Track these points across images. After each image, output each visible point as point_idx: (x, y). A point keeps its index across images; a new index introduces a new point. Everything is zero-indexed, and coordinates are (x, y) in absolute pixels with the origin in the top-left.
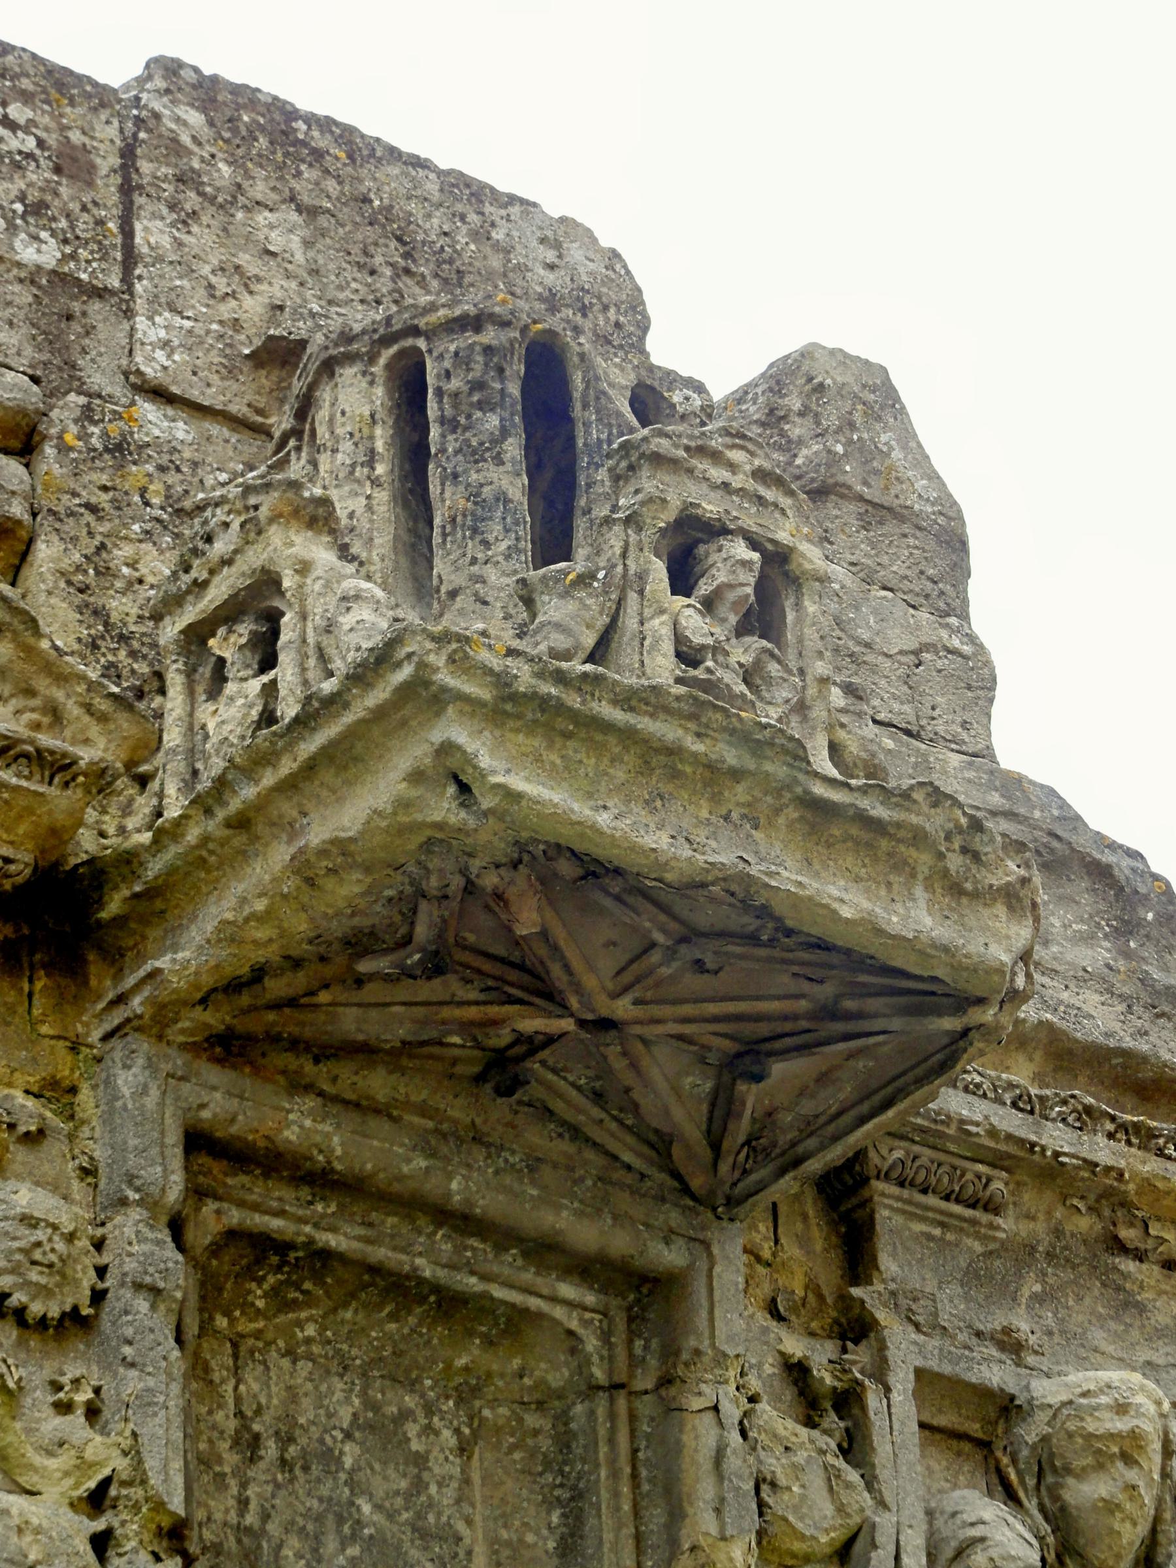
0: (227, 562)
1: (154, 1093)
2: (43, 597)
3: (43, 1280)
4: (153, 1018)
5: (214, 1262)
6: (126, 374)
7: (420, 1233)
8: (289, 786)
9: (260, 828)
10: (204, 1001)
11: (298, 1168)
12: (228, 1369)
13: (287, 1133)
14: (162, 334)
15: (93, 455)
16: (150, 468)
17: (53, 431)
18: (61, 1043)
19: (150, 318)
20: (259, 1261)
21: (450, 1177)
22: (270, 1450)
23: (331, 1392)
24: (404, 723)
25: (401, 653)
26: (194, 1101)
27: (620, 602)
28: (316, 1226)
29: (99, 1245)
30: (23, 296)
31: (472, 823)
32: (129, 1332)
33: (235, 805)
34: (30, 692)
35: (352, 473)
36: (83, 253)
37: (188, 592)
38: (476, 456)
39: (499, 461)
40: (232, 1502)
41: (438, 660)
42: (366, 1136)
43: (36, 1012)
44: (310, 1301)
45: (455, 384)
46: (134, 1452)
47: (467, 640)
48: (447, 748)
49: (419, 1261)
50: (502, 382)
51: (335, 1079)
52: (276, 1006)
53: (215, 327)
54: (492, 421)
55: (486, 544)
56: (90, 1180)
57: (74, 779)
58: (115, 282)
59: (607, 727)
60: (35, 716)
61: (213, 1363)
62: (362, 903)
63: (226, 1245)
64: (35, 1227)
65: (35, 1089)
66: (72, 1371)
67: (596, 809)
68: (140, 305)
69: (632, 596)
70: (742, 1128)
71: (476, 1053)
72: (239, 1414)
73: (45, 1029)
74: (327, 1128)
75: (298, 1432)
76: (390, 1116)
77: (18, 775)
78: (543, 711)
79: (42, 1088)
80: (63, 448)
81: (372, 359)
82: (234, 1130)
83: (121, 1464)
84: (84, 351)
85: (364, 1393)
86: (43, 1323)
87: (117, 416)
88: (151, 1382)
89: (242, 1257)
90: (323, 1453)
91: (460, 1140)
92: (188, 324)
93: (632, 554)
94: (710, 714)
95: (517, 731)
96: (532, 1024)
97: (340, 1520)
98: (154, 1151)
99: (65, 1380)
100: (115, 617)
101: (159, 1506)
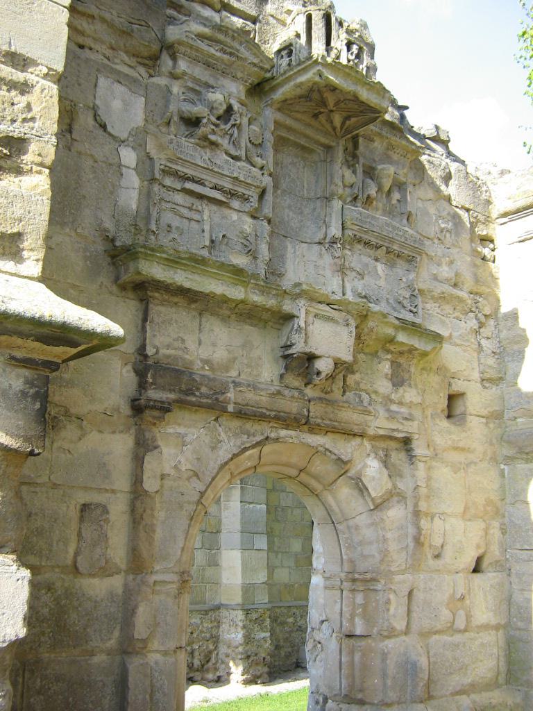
22: (280, 166)
29: (263, 135)
70: (345, 127)
81: (304, 13)
86: (255, 145)
94: (117, 20)
96: (322, 110)
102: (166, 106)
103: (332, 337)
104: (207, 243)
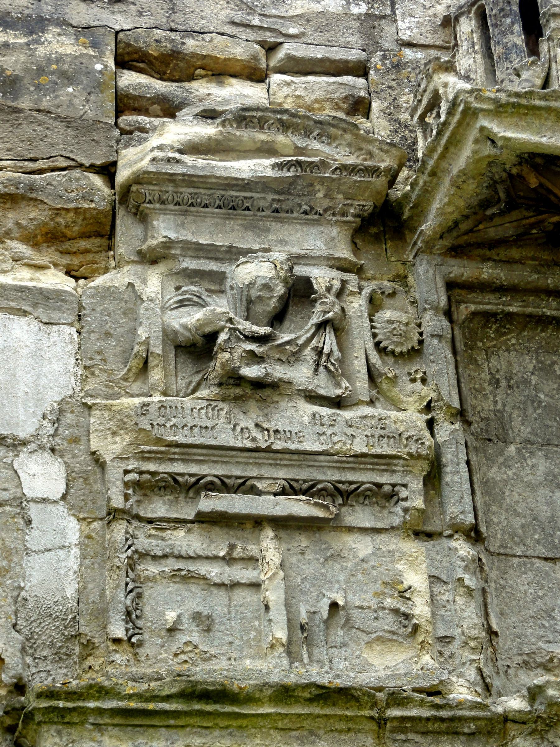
0: (425, 91)
1: (431, 272)
2: (375, 120)
3: (399, 340)
4: (426, 247)
5: (472, 325)
6: (397, 41)
7: (543, 300)
8: (443, 156)
9: (439, 174)
10: (441, 237)
11: (491, 287)
12: (484, 359)
13: (483, 276)
14: (408, 25)
15: (388, 70)
16: (409, 70)
17: (372, 65)
18: (399, 263)
19: (403, 21)
20: (488, 321)
21: (547, 279)
22: (504, 383)
23: (524, 360)
24: (468, 124)
25: (459, 101)
26: (447, 271)
27: (550, 68)
28: (503, 305)
29: (419, 325)
30: (356, 24)
31: (499, 152)
32: (431, 351)
33: (429, 168)
34: (361, 149)
35: (468, 52)
36: (376, 6)
37: (418, 105)
38: (504, 34)
39: (512, 33)
40: (491, 403)
41: (471, 99)
42: (513, 271)
43: (388, 254)
44: (510, 331)
45: (494, 11)
46: (437, 390)
47: (480, 90)
48: (482, 129)
49: (544, 310)
50: (510, 6)
51: (498, 255)
52: (466, 233)
53: (427, 18)
54: (509, 20)
55: (511, 62)
56: (415, 305)
57: (380, 173)
58: (389, 12)
59: (539, 108)
60: (364, 156)
61: (478, 358)
62: (478, 190)
63: (473, 318)
64: (393, 323)
65: (392, 279)
66: (414, 368)
67: (541, 137)
68: (399, 17)
69: (553, 64)
71: (543, 234)
72: (490, 373)
73: (393, 259)
74: (498, 271)
75: (513, 376)
76: (521, 263)
77: (360, 177)
78: (514, 108)
79: (394, 278)
80: (377, 70)
81: (469, 12)
82: (464, 278)
83: (433, 395)
84: (381, 37)
85: (537, 358)
87: (395, 55)
88: (441, 366)
89: (481, 321)
90: (524, 381)
91: (549, 266)
92: (417, 20)
93: (551, 50)
95: (507, 117)
97: (533, 402)
98: (434, 291)
99: (412, 371)
100: (402, 120)
101: (449, 406)
102: (133, 332)
104: (281, 634)
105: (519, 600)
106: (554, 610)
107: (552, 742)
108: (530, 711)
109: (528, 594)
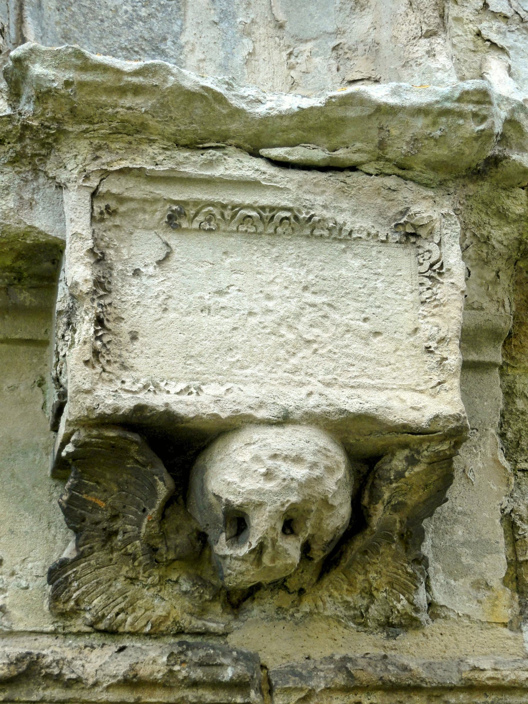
103: (309, 315)
105: (102, 21)
106: (165, 39)
107: (54, 178)
108: (9, 116)
109: (121, 12)
